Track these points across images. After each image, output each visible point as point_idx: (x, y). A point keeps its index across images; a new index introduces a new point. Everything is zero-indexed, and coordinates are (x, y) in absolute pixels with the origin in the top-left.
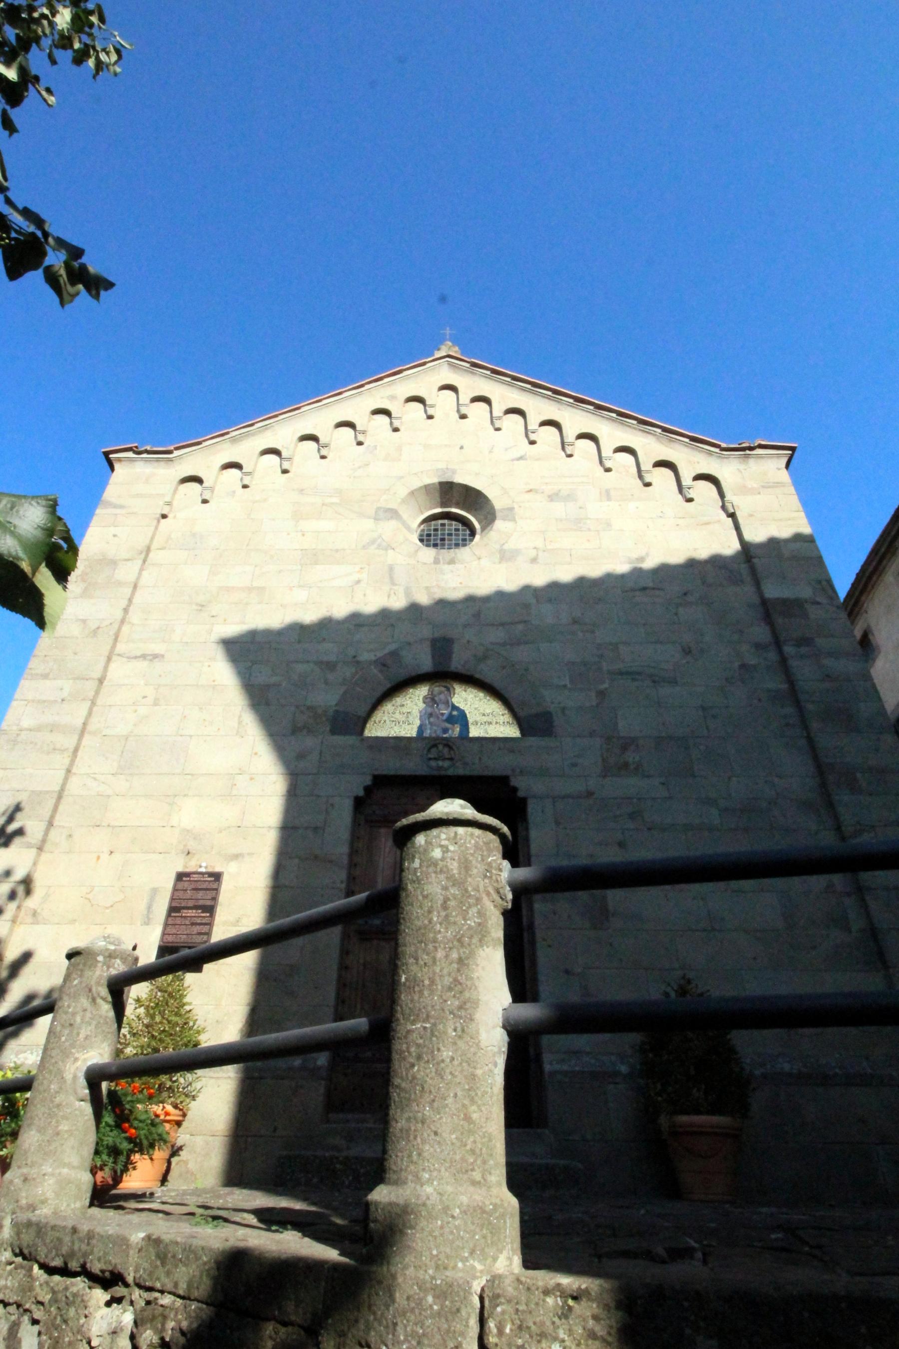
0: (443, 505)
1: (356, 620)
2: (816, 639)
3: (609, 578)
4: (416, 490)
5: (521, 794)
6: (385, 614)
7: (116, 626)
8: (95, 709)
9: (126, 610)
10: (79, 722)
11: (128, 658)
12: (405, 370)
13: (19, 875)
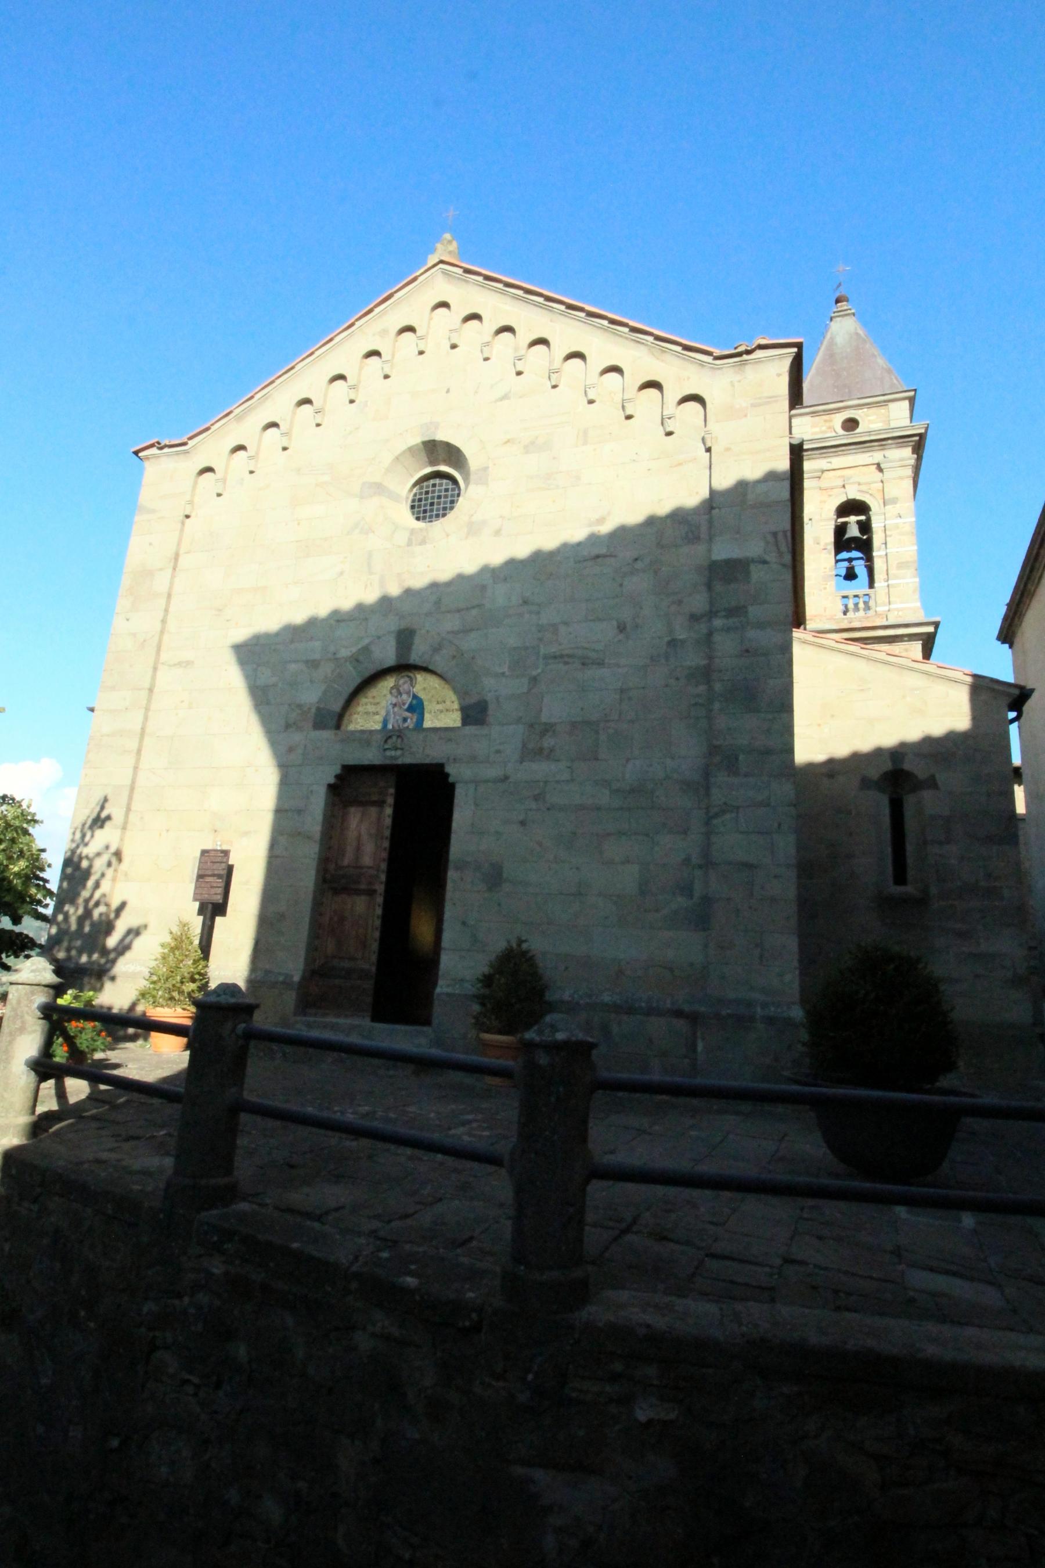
0: (432, 463)
1: (337, 618)
2: (750, 609)
3: (565, 549)
4: (400, 455)
5: (451, 780)
6: (360, 608)
7: (156, 638)
8: (150, 713)
9: (164, 621)
10: (138, 728)
11: (170, 666)
12: (396, 292)
13: (113, 849)
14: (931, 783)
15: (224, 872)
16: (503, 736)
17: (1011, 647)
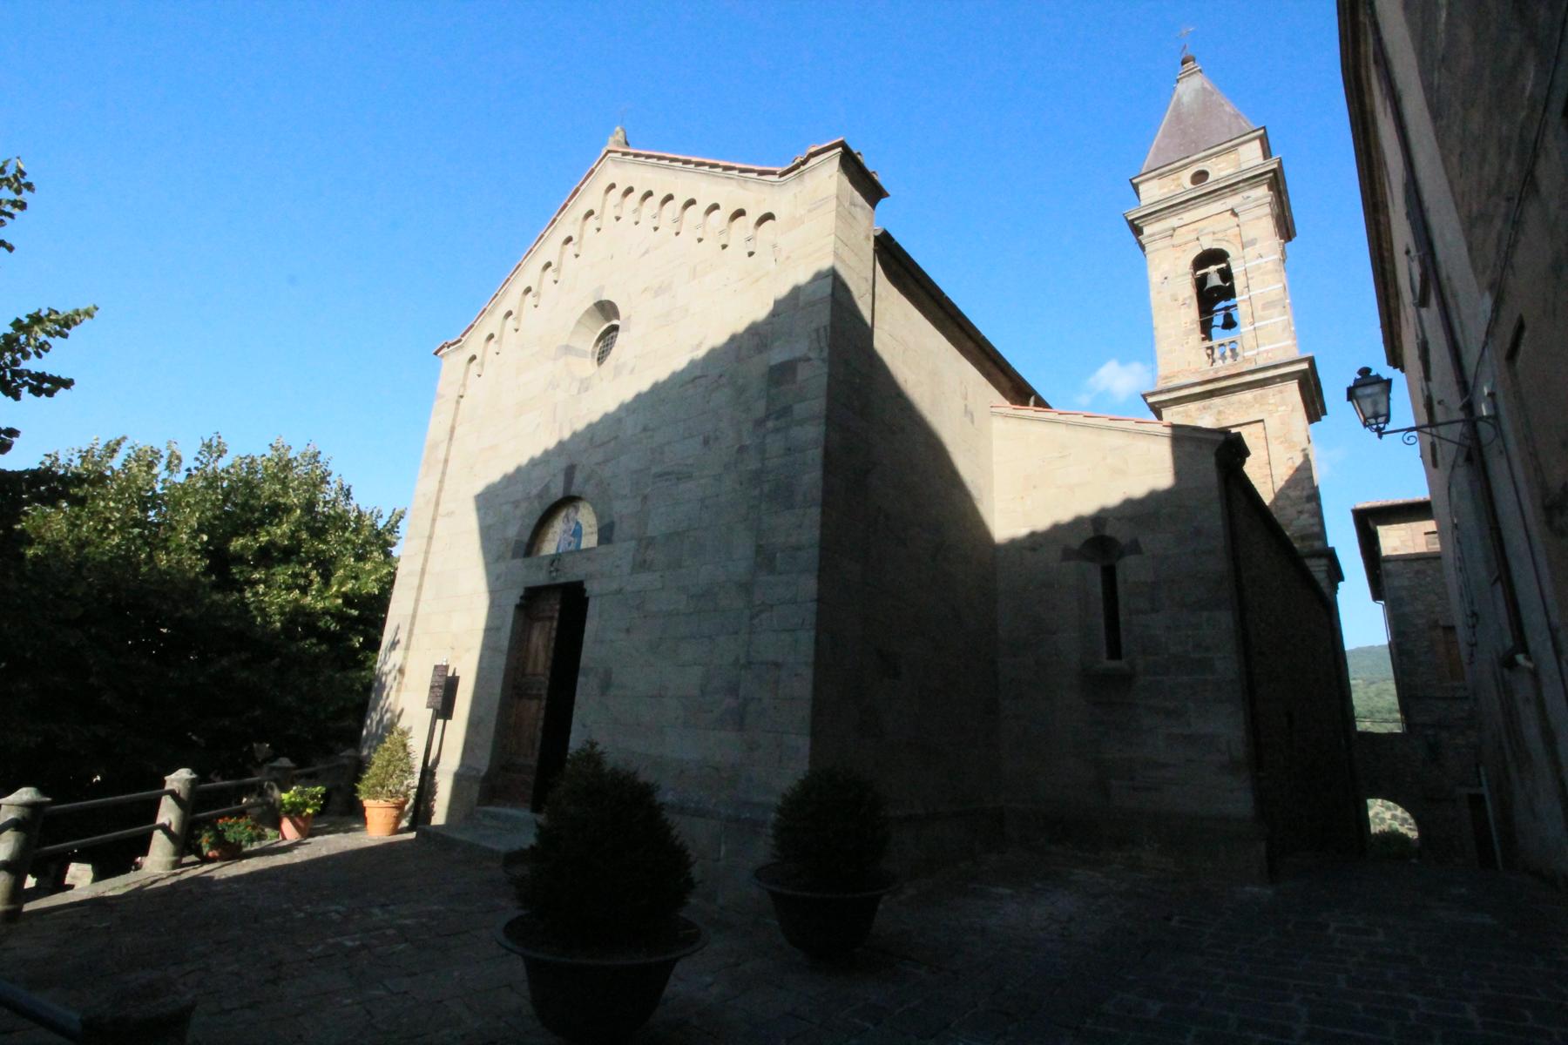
1: (534, 463)
3: (675, 377)
14: (1135, 548)
15: (1386, 582)
16: (623, 550)
17: (1403, 370)
